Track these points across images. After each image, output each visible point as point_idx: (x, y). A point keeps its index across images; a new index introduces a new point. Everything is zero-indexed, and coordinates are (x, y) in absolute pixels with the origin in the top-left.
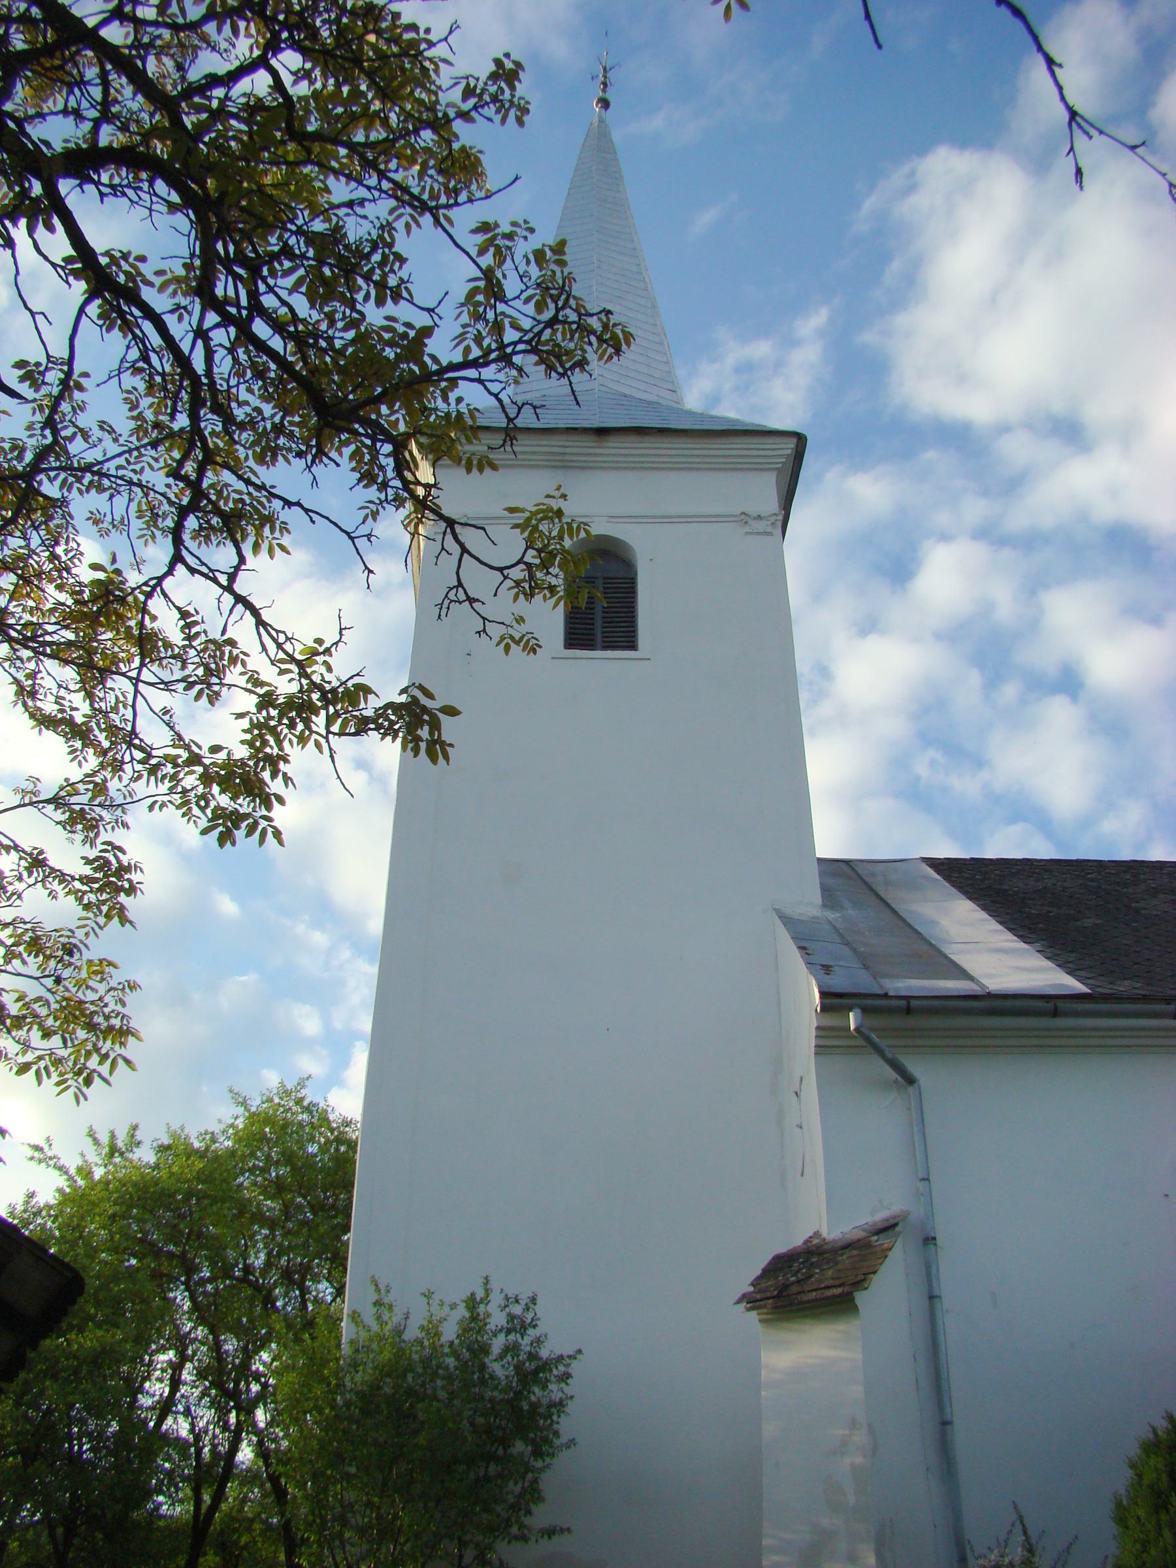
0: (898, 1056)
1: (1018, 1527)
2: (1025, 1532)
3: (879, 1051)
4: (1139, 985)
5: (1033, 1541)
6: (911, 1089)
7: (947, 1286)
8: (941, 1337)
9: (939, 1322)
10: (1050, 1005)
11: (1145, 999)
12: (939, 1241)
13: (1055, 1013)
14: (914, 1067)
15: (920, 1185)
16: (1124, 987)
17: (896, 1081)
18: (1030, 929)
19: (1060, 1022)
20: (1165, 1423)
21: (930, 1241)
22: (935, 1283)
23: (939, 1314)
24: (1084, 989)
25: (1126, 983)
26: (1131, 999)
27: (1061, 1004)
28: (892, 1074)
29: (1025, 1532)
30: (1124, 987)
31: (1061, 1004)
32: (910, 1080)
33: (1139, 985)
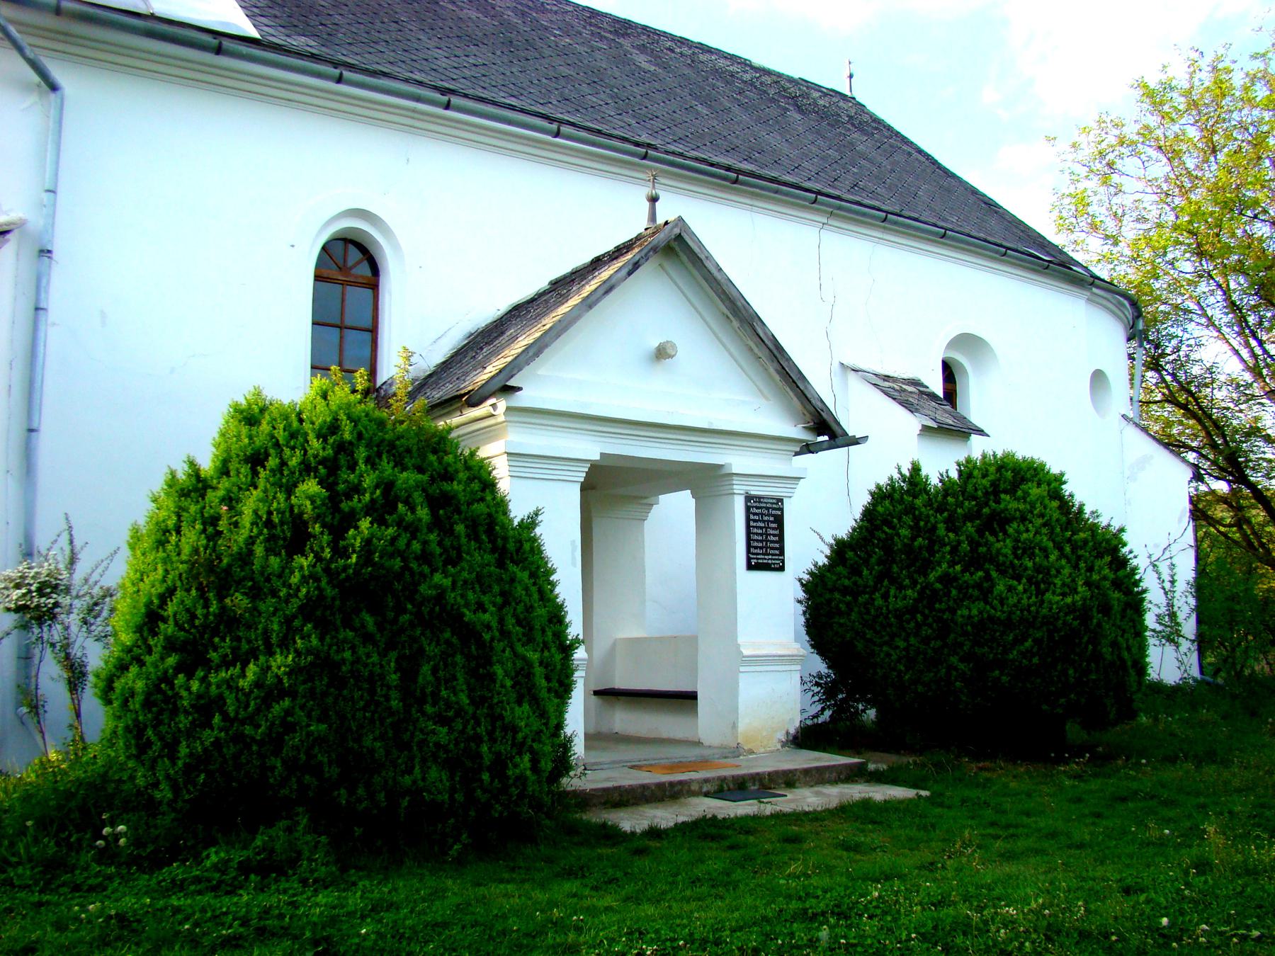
0: (42, 59)
1: (66, 536)
2: (71, 542)
3: (20, 50)
4: (313, 43)
6: (52, 96)
7: (56, 301)
8: (41, 349)
9: (41, 335)
10: (215, 42)
11: (313, 57)
13: (219, 51)
14: (58, 72)
15: (46, 196)
16: (298, 42)
17: (39, 86)
18: (1242, 321)
19: (449, 113)
20: (186, 467)
21: (45, 253)
22: (43, 295)
23: (42, 327)
24: (255, 34)
25: (303, 39)
26: (299, 55)
27: (227, 44)
28: (36, 78)
29: (71, 542)
30: (298, 42)
31: (227, 44)
32: (54, 88)
33: (313, 43)
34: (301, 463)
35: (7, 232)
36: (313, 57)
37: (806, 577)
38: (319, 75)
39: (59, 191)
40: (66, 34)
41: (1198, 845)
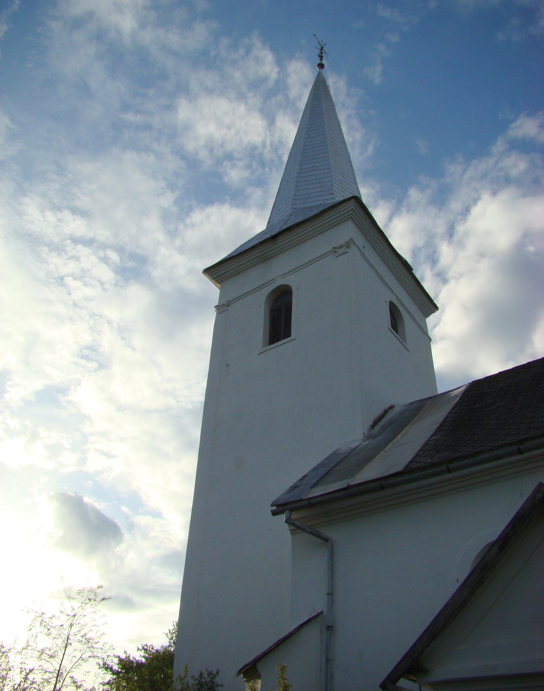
14: (327, 532)
36: (433, 465)
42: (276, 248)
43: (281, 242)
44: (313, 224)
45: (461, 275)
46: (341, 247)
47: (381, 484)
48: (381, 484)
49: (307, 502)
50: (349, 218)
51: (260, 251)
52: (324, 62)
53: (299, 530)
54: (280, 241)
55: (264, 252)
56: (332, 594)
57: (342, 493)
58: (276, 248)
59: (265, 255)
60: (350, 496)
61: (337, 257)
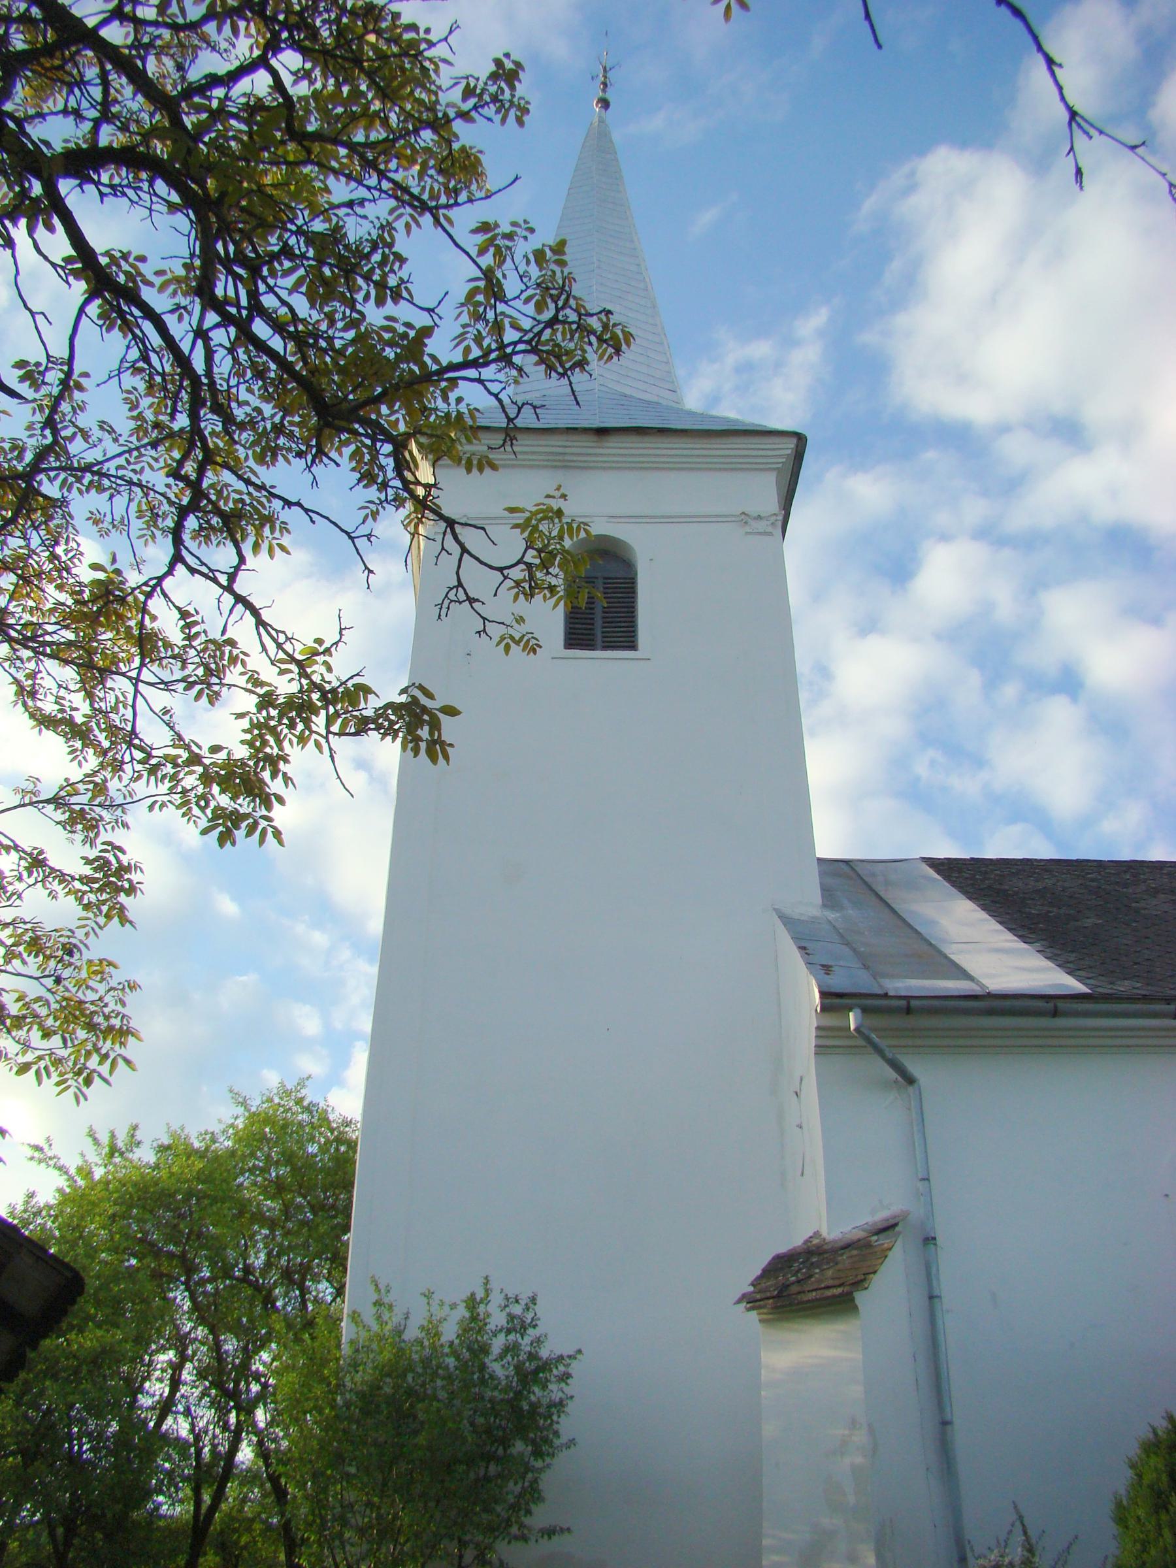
0: (898, 1056)
2: (1025, 1533)
3: (879, 1051)
4: (1139, 985)
5: (1033, 1541)
6: (911, 1089)
7: (946, 1285)
8: (941, 1337)
9: (939, 1322)
10: (1050, 1005)
11: (1145, 998)
12: (939, 1241)
13: (1055, 1013)
14: (914, 1066)
15: (920, 1185)
16: (1124, 987)
17: (896, 1081)
20: (1165, 1423)
22: (935, 1283)
23: (939, 1315)
24: (1084, 989)
25: (1127, 983)
26: (1131, 999)
27: (1061, 1005)
28: (893, 1074)
29: (1025, 1533)
31: (1061, 1005)
32: (910, 1081)
33: (1139, 985)
34: (362, 1395)
35: (895, 1225)
36: (1145, 998)
37: (555, 1391)
38: (1155, 1015)
39: (931, 1179)
40: (913, 1030)
41: (255, 1183)
42: (596, 455)
43: (614, 447)
44: (541, 443)
45: (72, 662)
46: (759, 517)
47: (1055, 1007)
48: (1055, 1007)
49: (903, 1003)
50: (774, 469)
51: (560, 443)
52: (609, 96)
53: (870, 1049)
54: (611, 445)
55: (568, 450)
56: (928, 1179)
57: (1040, 1004)
58: (596, 455)
59: (567, 458)
60: (991, 1012)
61: (747, 533)
